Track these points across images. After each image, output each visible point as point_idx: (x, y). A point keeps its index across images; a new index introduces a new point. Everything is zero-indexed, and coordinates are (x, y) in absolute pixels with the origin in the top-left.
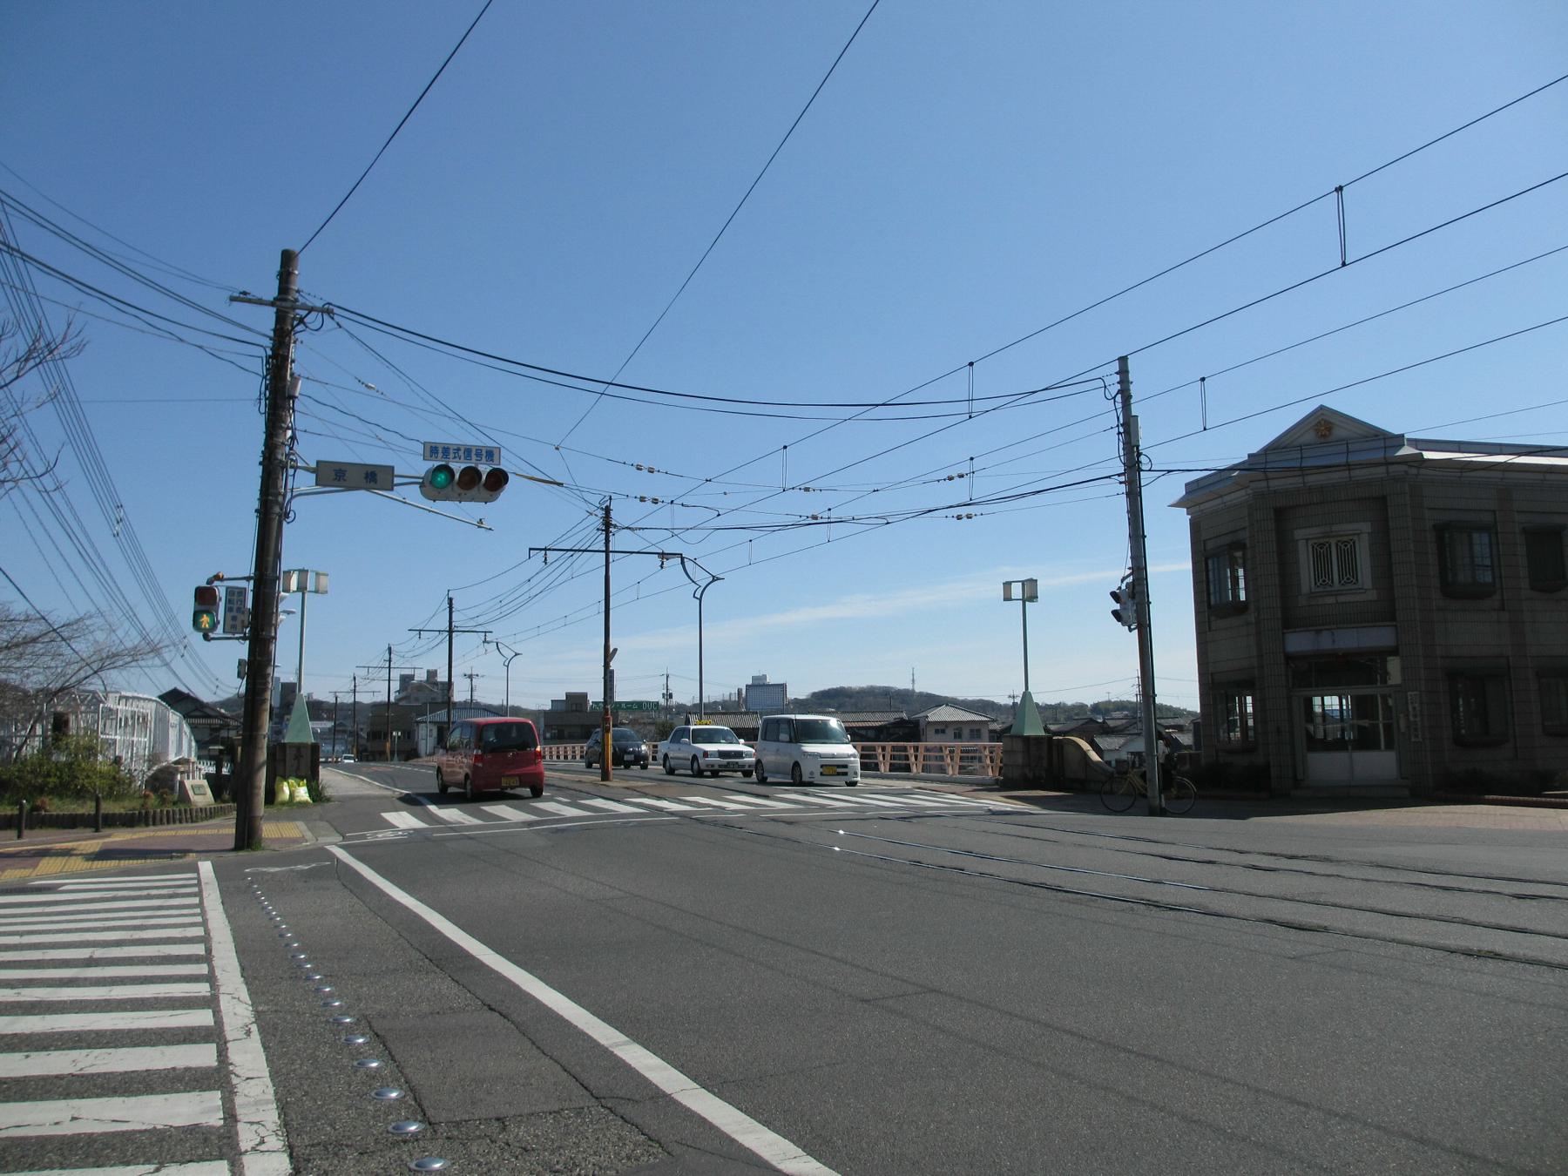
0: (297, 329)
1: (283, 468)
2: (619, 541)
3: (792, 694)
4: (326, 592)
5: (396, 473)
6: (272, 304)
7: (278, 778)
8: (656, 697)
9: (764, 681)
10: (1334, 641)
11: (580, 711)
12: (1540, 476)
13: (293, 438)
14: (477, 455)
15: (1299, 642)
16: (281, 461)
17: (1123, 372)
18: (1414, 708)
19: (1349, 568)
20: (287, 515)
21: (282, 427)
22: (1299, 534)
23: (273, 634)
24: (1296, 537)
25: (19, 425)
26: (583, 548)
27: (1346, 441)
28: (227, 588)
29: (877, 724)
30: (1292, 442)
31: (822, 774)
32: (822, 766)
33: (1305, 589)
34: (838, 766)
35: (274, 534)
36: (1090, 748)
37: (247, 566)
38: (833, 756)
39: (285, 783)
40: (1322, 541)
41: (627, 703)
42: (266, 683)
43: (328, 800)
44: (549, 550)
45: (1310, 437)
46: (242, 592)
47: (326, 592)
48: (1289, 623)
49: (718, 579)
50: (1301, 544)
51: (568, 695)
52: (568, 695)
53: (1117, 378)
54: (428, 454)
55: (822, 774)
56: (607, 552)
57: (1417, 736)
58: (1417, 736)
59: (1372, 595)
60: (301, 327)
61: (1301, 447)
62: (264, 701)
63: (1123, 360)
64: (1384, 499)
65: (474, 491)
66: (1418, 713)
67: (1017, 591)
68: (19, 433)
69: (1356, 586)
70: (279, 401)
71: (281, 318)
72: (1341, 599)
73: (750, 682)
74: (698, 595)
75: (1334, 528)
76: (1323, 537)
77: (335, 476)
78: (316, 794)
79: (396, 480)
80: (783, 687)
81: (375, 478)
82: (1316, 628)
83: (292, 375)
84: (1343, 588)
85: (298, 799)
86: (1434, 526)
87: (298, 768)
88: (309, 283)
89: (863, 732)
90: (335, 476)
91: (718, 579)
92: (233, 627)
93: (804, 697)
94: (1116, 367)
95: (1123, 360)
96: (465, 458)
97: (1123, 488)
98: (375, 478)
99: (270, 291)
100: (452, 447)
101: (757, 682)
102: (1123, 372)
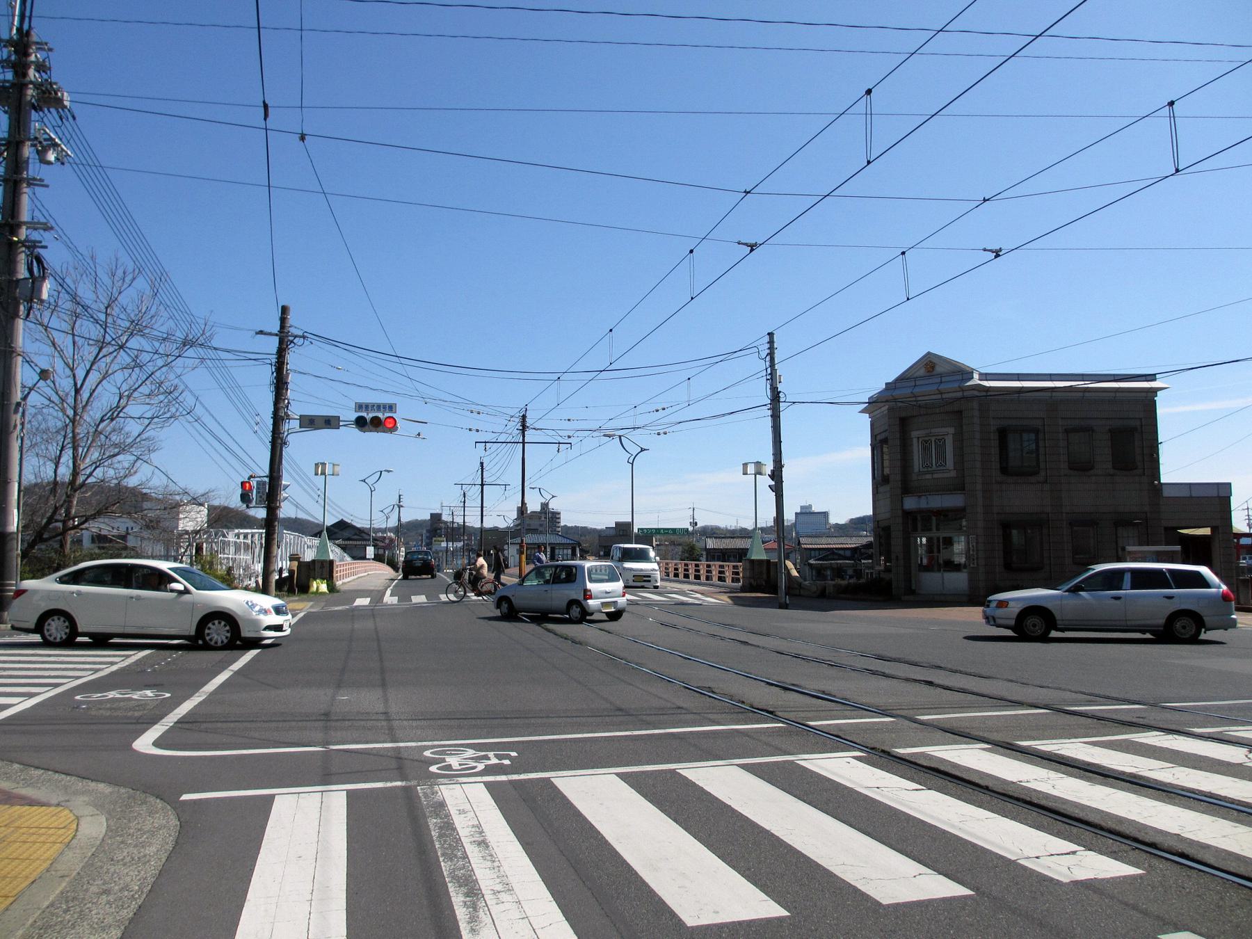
0: (289, 347)
1: (283, 420)
2: (530, 435)
3: (834, 519)
4: (338, 475)
5: (341, 419)
6: (276, 335)
7: (311, 579)
8: (686, 525)
9: (810, 510)
10: (927, 503)
11: (626, 535)
12: (1081, 394)
13: (289, 403)
14: (384, 408)
15: (910, 503)
16: (281, 416)
17: (771, 342)
18: (973, 546)
19: (941, 455)
20: (285, 443)
21: (281, 399)
22: (914, 434)
23: (278, 505)
24: (912, 436)
25: (180, 384)
26: (505, 444)
27: (941, 375)
28: (257, 482)
29: (853, 546)
30: (912, 375)
31: (634, 581)
32: (634, 576)
33: (916, 470)
34: (645, 576)
35: (278, 453)
36: (792, 566)
37: (266, 470)
38: (642, 570)
39: (315, 582)
40: (927, 439)
41: (664, 529)
42: (275, 530)
43: (338, 592)
44: (488, 442)
45: (922, 372)
46: (264, 483)
47: (338, 475)
48: (906, 489)
49: (645, 450)
50: (915, 441)
51: (617, 524)
52: (617, 524)
53: (768, 346)
54: (357, 409)
55: (634, 581)
56: (524, 443)
57: (974, 564)
58: (974, 564)
59: (953, 474)
60: (292, 345)
61: (915, 379)
62: (274, 539)
63: (771, 335)
64: (960, 412)
65: (367, 428)
66: (975, 549)
67: (751, 469)
68: (182, 387)
69: (944, 468)
70: (280, 385)
71: (281, 342)
72: (935, 476)
73: (799, 511)
74: (631, 461)
75: (933, 431)
76: (926, 437)
77: (310, 422)
78: (332, 588)
79: (341, 423)
80: (825, 515)
81: (330, 422)
82: (918, 494)
83: (287, 370)
84: (939, 469)
85: (320, 591)
86: (998, 429)
87: (322, 574)
88: (296, 323)
89: (841, 552)
90: (310, 422)
91: (645, 450)
92: (260, 501)
93: (843, 523)
94: (767, 339)
95: (771, 335)
96: (378, 410)
97: (769, 412)
98: (330, 422)
99: (276, 328)
100: (370, 405)
101: (804, 511)
102: (771, 342)
